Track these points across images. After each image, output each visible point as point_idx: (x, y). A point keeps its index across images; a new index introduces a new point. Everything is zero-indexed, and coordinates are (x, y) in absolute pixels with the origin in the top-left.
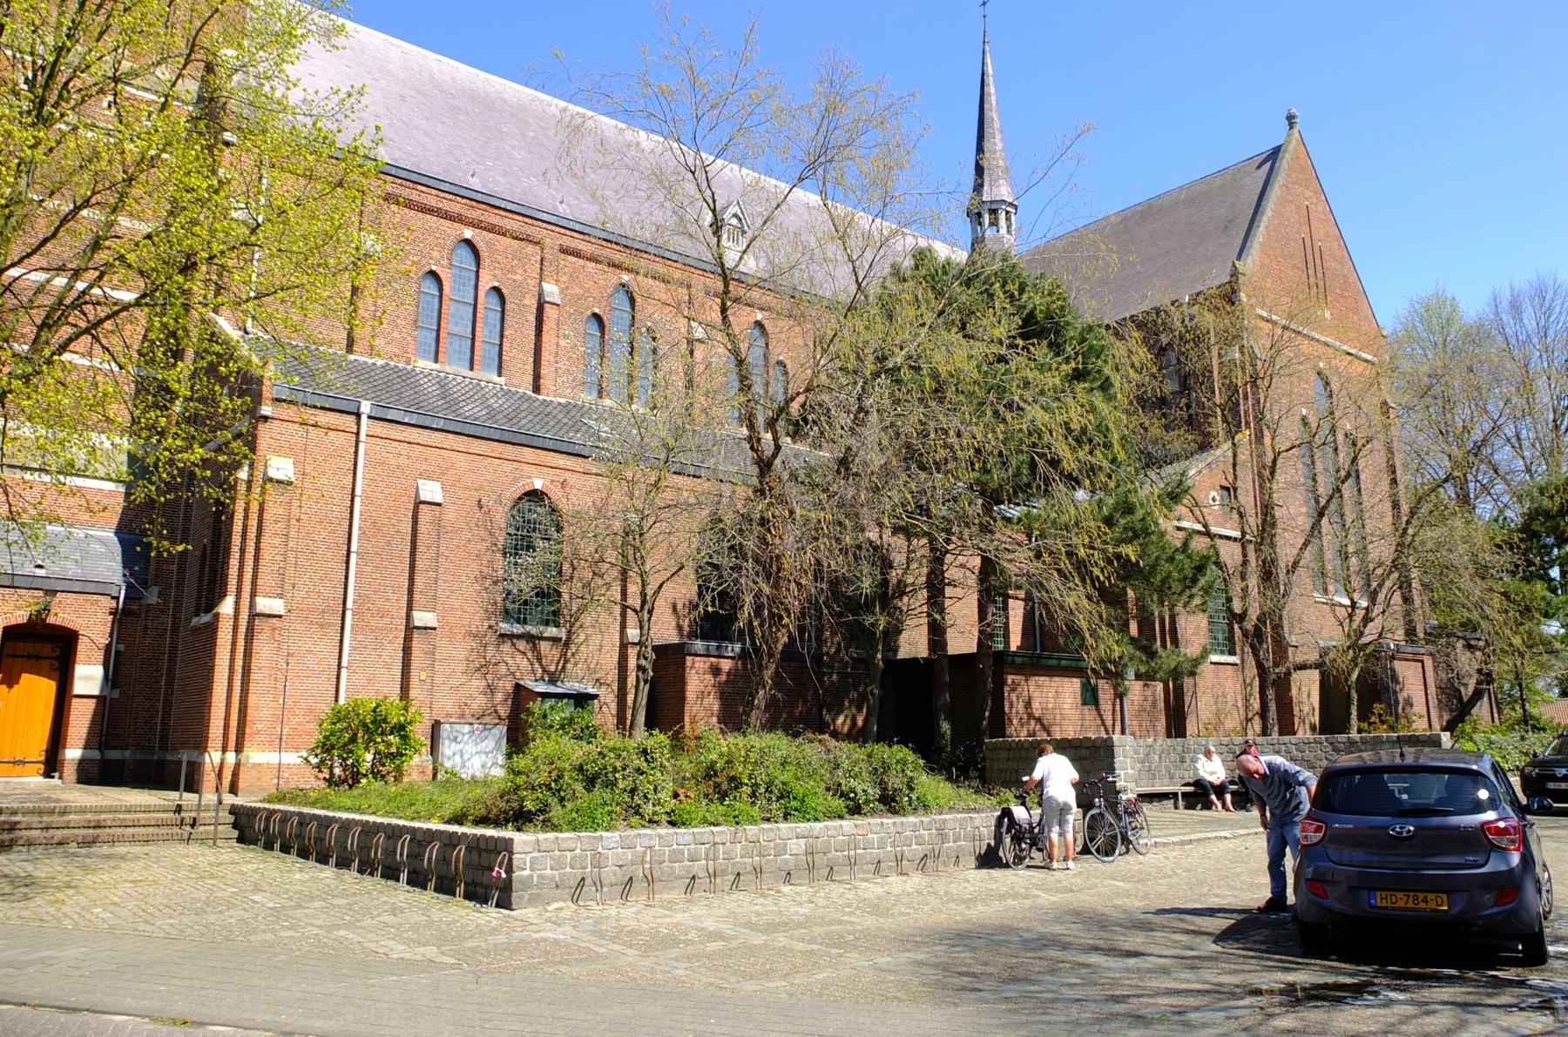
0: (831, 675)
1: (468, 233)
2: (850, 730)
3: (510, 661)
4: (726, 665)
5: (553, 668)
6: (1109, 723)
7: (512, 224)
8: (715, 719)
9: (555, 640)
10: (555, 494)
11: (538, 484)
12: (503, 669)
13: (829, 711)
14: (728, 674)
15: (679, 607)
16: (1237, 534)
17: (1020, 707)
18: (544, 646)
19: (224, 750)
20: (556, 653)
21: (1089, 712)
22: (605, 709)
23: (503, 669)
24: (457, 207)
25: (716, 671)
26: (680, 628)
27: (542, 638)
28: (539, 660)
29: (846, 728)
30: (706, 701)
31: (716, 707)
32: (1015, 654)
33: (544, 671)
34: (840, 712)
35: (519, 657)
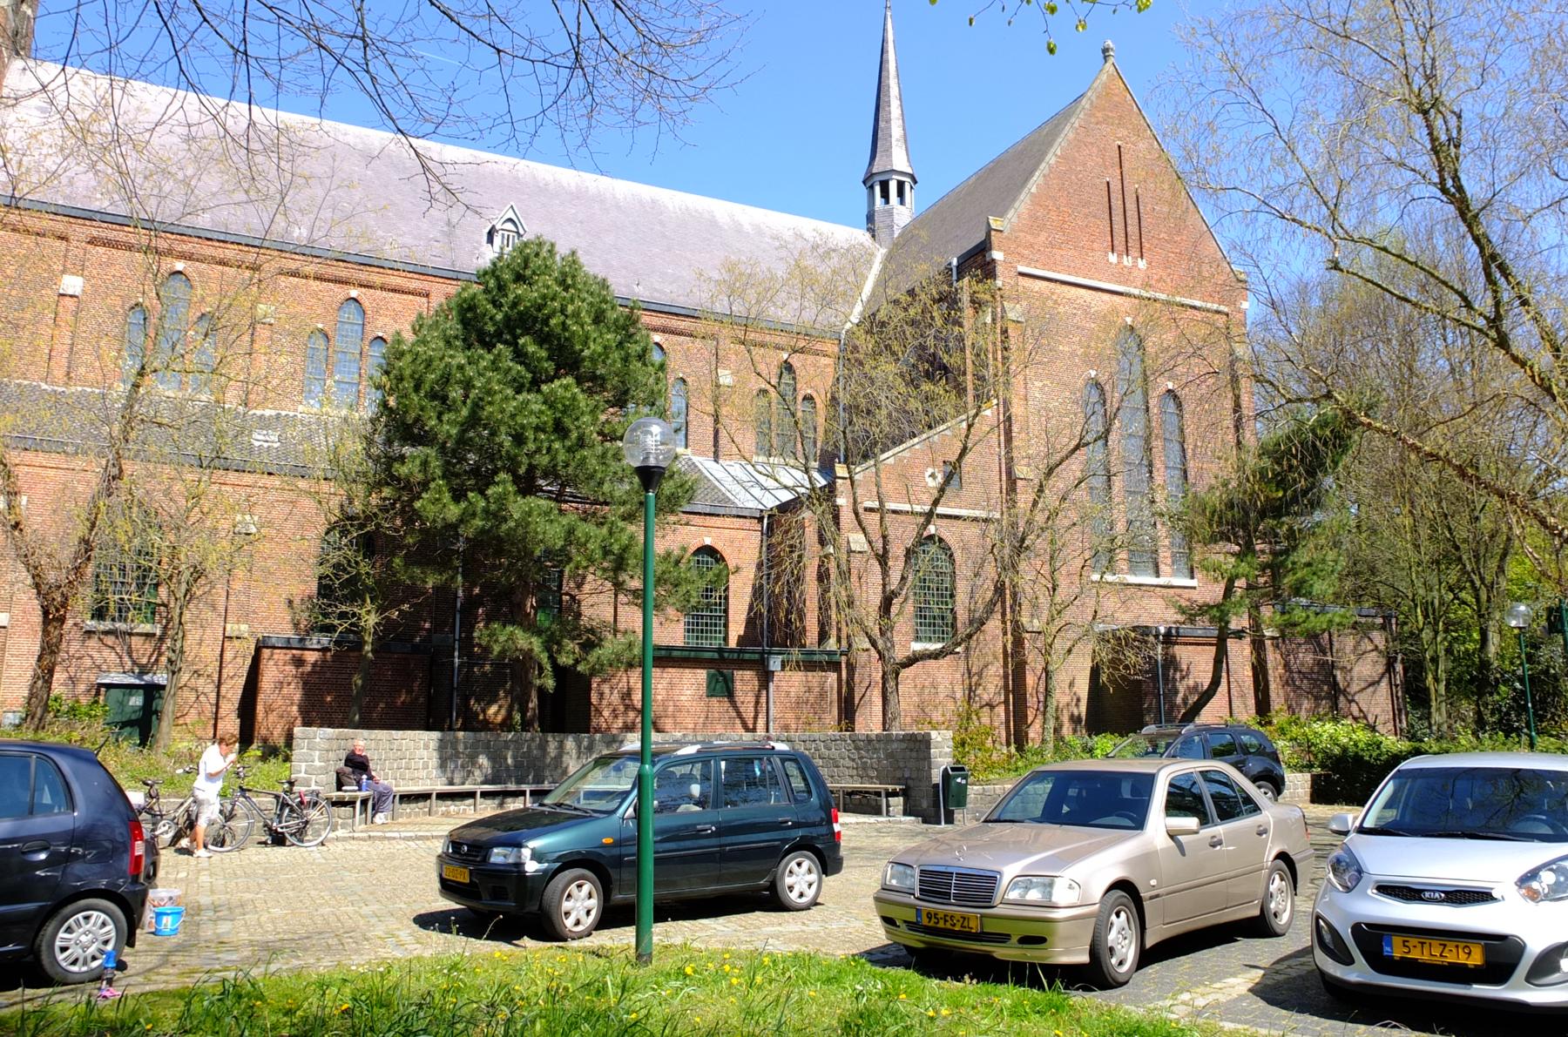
0: (482, 666)
1: (354, 293)
2: (504, 720)
3: (95, 655)
4: (312, 657)
5: (144, 661)
6: (749, 714)
7: (208, 250)
8: (295, 708)
9: (148, 635)
10: (726, 552)
11: (708, 541)
12: (88, 662)
13: (478, 701)
14: (314, 665)
15: (297, 601)
16: (876, 505)
17: (615, 698)
18: (136, 642)
19: (1008, 744)
20: (149, 647)
21: (719, 706)
22: (202, 698)
23: (88, 662)
24: (341, 271)
25: (299, 662)
26: (296, 625)
27: (131, 634)
28: (130, 654)
29: (499, 718)
30: (285, 691)
31: (298, 696)
32: (732, 651)
33: (134, 663)
34: (490, 703)
35: (106, 652)
